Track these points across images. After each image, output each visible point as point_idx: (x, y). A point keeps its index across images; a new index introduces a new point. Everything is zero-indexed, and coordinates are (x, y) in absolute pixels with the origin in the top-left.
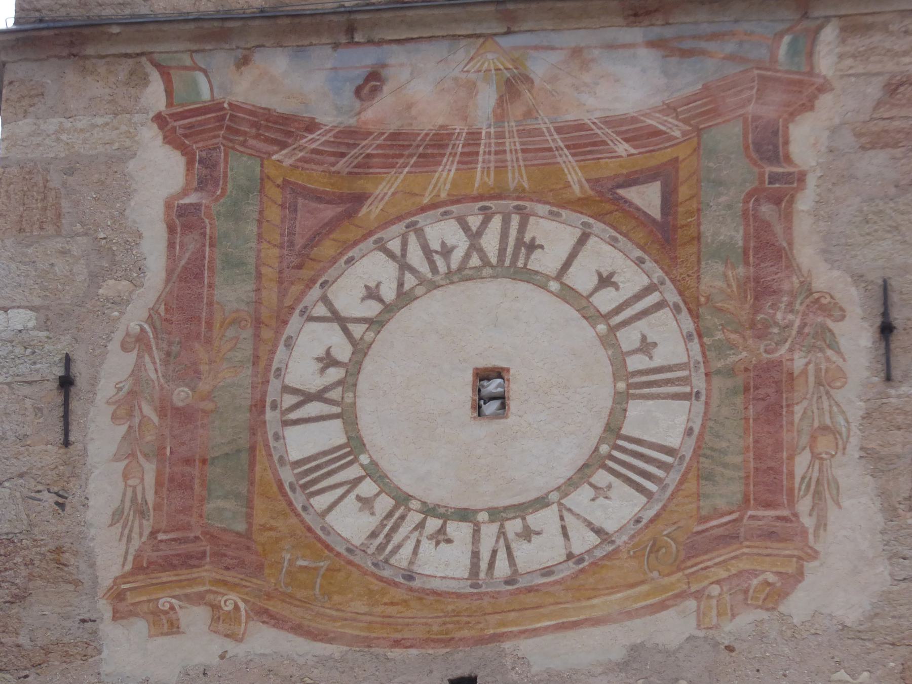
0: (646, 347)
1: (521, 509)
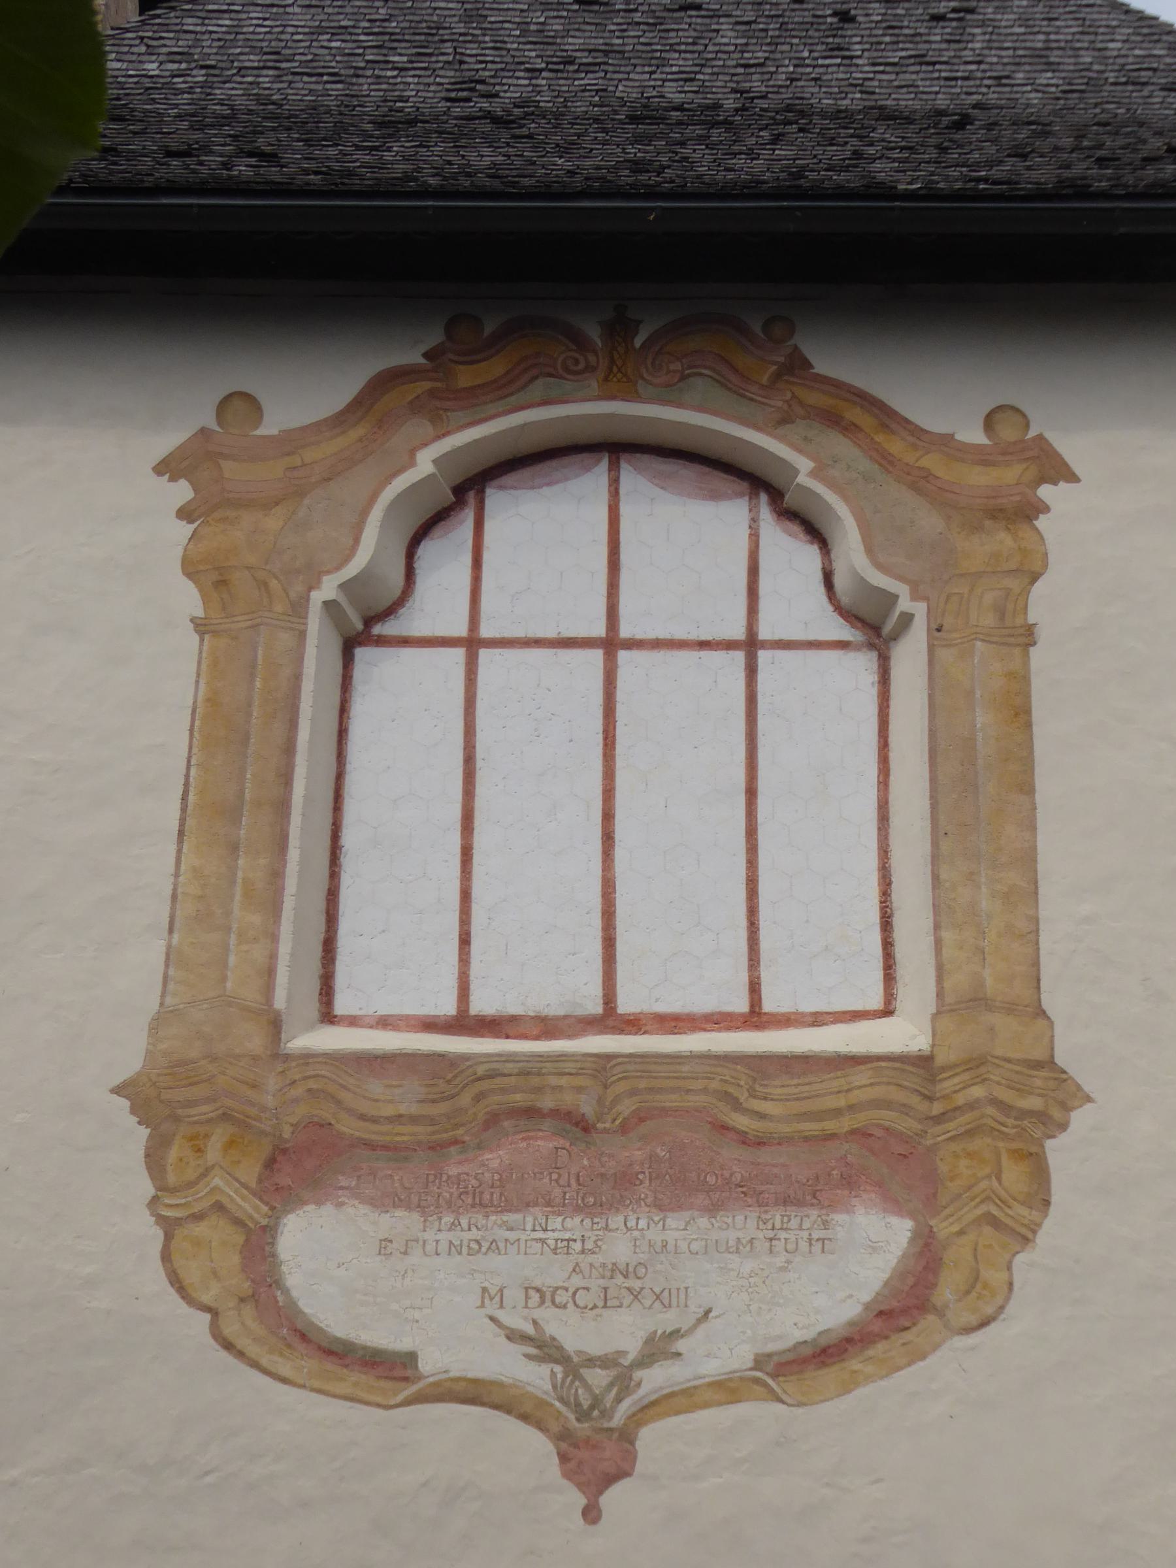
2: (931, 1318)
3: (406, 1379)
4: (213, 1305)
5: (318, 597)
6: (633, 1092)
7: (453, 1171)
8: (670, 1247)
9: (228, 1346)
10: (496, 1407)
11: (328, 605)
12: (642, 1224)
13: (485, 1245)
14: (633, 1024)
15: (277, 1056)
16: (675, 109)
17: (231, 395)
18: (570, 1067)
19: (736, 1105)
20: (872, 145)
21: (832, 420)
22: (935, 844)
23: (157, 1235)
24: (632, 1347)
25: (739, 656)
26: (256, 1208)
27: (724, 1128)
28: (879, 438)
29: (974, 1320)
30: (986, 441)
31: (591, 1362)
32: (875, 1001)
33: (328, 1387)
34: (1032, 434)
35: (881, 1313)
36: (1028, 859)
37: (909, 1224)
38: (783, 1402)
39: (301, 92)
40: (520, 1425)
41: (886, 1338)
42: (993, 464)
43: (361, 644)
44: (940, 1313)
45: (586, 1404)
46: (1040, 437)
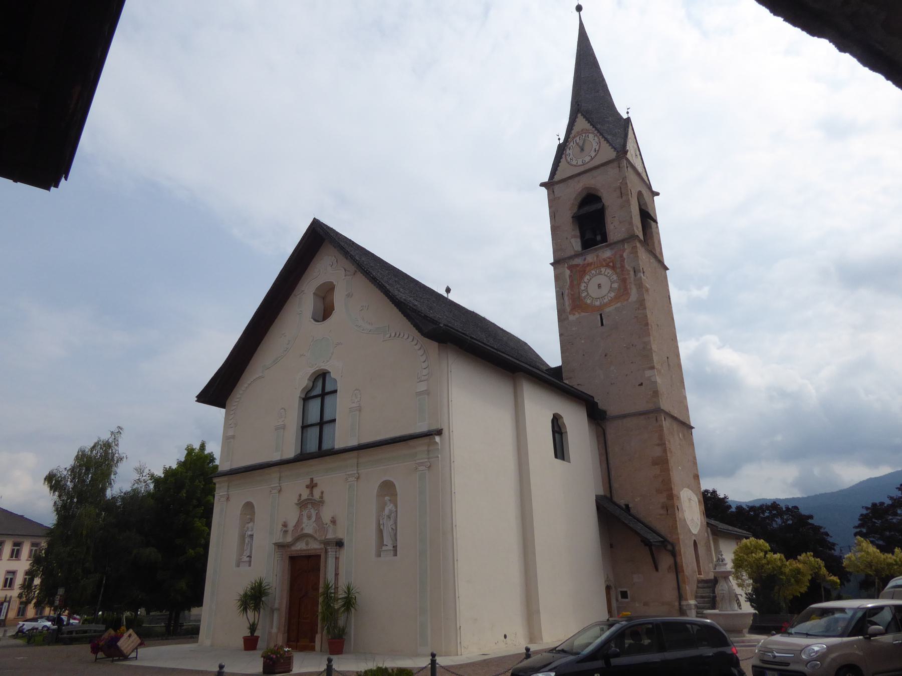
0: (613, 279)
1: (604, 297)
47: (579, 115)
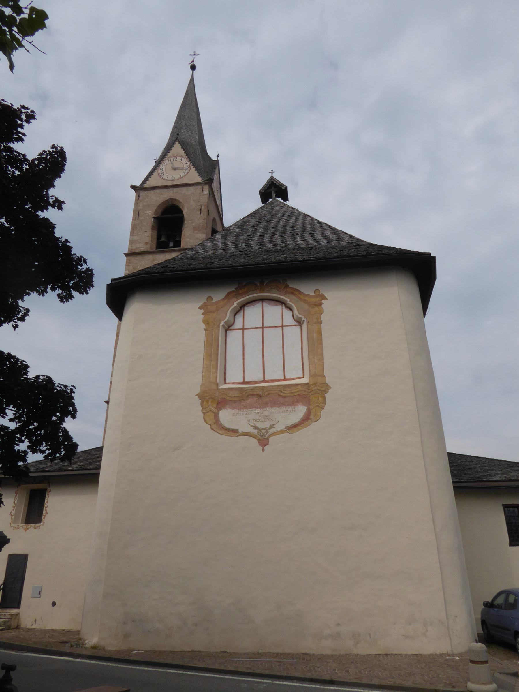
2: (310, 420)
3: (237, 433)
4: (211, 424)
5: (221, 324)
6: (267, 391)
7: (242, 403)
8: (273, 412)
9: (213, 430)
10: (249, 436)
11: (222, 325)
12: (269, 409)
13: (247, 414)
14: (268, 381)
15: (218, 389)
16: (271, 250)
17: (209, 297)
18: (258, 388)
19: (281, 392)
20: (298, 253)
21: (292, 293)
22: (309, 353)
23: (203, 415)
24: (268, 427)
25: (281, 328)
26: (216, 410)
27: (280, 395)
28: (299, 295)
29: (316, 420)
30: (314, 295)
31: (263, 429)
32: (302, 376)
33: (226, 434)
34: (321, 293)
35: (303, 420)
36: (322, 354)
37: (306, 407)
38: (289, 433)
39: (219, 253)
40: (253, 438)
41: (303, 423)
42: (315, 298)
43: (228, 330)
44: (311, 419)
45: (262, 435)
46: (322, 294)
47: (177, 143)
